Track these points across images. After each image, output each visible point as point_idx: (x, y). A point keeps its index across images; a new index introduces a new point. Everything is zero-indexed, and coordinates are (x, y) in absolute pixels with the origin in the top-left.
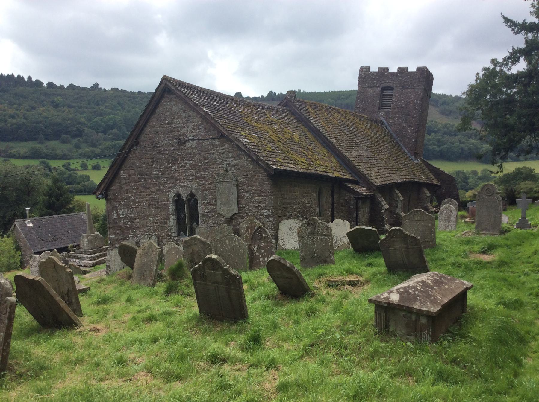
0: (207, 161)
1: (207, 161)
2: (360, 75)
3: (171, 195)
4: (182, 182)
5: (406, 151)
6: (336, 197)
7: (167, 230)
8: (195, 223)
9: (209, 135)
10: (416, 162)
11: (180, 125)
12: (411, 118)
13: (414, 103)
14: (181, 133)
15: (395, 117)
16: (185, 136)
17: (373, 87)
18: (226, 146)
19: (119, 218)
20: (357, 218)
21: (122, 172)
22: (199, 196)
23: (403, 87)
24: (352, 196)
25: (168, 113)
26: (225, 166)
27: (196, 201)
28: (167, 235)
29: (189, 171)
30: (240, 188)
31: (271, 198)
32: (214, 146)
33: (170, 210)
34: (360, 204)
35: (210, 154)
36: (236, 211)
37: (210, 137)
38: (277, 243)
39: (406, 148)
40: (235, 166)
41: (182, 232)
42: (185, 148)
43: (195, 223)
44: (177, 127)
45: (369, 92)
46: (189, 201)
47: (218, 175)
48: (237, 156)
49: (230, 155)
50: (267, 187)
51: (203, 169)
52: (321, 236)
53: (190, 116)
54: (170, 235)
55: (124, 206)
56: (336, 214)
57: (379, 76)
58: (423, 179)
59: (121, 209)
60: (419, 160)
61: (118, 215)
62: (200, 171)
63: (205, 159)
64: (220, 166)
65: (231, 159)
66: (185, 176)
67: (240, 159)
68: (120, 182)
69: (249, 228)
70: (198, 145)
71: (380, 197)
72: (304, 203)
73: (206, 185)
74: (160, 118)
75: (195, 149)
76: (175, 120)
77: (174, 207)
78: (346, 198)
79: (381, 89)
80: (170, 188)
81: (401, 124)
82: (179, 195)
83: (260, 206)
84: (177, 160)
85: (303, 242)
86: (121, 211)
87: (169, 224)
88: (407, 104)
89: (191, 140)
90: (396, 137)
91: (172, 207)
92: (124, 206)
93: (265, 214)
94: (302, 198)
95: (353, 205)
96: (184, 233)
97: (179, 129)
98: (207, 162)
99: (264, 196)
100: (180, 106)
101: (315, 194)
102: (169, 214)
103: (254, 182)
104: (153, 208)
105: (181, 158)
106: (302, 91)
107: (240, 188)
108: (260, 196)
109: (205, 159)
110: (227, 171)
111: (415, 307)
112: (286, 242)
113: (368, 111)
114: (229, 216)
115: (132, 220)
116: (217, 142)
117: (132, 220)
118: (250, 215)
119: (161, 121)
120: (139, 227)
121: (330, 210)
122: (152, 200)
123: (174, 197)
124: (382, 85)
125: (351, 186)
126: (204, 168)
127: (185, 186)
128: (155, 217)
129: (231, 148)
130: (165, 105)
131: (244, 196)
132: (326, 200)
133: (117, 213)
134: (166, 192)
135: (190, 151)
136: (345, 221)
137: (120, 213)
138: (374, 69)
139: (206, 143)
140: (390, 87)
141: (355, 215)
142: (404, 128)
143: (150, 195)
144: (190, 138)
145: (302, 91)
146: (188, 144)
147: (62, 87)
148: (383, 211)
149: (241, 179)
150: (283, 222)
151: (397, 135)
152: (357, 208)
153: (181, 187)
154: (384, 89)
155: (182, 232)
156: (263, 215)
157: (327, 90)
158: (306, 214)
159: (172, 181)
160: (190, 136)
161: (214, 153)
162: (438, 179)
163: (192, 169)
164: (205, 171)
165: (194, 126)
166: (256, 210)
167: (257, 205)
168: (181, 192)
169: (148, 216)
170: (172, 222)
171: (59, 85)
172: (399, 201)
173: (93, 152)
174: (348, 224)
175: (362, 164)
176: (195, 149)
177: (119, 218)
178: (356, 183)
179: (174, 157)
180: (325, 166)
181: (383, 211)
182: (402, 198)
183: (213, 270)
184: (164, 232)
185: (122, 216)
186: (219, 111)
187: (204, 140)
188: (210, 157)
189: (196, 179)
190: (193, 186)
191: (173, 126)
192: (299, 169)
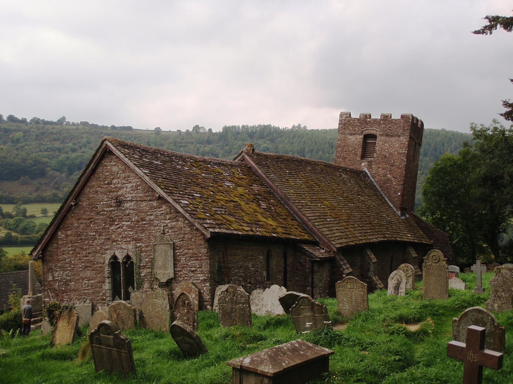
0: (144, 222)
1: (144, 222)
2: (340, 121)
3: (108, 257)
4: (119, 244)
5: (392, 206)
6: (290, 260)
7: (101, 294)
8: (130, 287)
9: (147, 196)
10: (403, 218)
11: (119, 185)
12: (396, 169)
13: (398, 153)
14: (120, 193)
15: (379, 167)
16: (124, 196)
17: (354, 134)
18: (164, 207)
19: (54, 280)
20: (313, 282)
21: (59, 233)
23: (387, 135)
24: (308, 259)
25: (108, 174)
26: (162, 228)
28: (101, 299)
29: (126, 233)
30: (177, 251)
31: (207, 262)
32: (152, 207)
33: (106, 273)
34: (316, 268)
35: (148, 215)
36: (172, 276)
37: (149, 198)
38: (212, 309)
39: (391, 202)
40: (172, 228)
41: (117, 296)
42: (123, 208)
43: (130, 287)
44: (117, 187)
46: (125, 263)
47: (155, 237)
48: (175, 218)
49: (168, 217)
50: (204, 251)
51: (141, 230)
52: (240, 303)
53: (129, 177)
54: (105, 300)
55: (60, 267)
57: (360, 123)
58: (408, 237)
59: (57, 271)
60: (407, 216)
61: (54, 277)
62: (136, 233)
63: (143, 220)
64: (157, 228)
65: (169, 221)
66: (122, 238)
67: (177, 221)
68: (57, 243)
70: (136, 206)
71: (342, 260)
72: (248, 267)
73: (143, 248)
74: (100, 178)
75: (134, 210)
76: (115, 181)
77: (109, 269)
78: (302, 261)
79: (363, 136)
80: (107, 249)
81: (385, 176)
82: (115, 257)
83: (196, 270)
84: (114, 221)
85: (222, 309)
86: (57, 274)
87: (104, 287)
88: (391, 154)
89: (129, 201)
90: (380, 190)
91: (107, 269)
92: (60, 267)
93: (201, 278)
94: (245, 262)
95: (308, 269)
96: (119, 297)
98: (145, 224)
99: (201, 260)
100: (120, 167)
101: (261, 257)
103: (191, 245)
104: (88, 270)
105: (119, 219)
107: (177, 251)
109: (143, 220)
110: (164, 234)
111: (259, 369)
114: (164, 280)
115: (66, 283)
116: (155, 204)
117: (66, 283)
118: (186, 280)
119: (100, 181)
120: (74, 290)
121: (282, 274)
122: (88, 262)
123: (110, 259)
124: (365, 133)
126: (142, 230)
127: (121, 248)
128: (90, 280)
129: (168, 210)
130: (106, 166)
131: (180, 260)
132: (276, 262)
133: (53, 275)
134: (102, 254)
135: (127, 212)
136: (282, 287)
137: (56, 275)
138: (355, 115)
139: (144, 204)
141: (310, 280)
142: (388, 180)
143: (86, 256)
144: (128, 199)
146: (127, 205)
147: (24, 121)
148: (344, 275)
149: (178, 242)
151: (381, 188)
152: (313, 272)
153: (118, 249)
154: (367, 137)
155: (117, 296)
156: (199, 280)
159: (109, 242)
160: (129, 197)
161: (151, 215)
162: (430, 238)
163: (129, 231)
164: (142, 233)
165: (132, 186)
166: (193, 275)
167: (193, 269)
168: (118, 254)
169: (83, 279)
170: (107, 286)
171: (21, 119)
172: (371, 263)
173: (55, 195)
175: (326, 222)
176: (134, 210)
177: (54, 280)
179: (112, 218)
180: (271, 226)
181: (344, 275)
182: (375, 260)
183: (107, 335)
184: (98, 296)
185: (57, 278)
186: (161, 170)
187: (142, 201)
188: (147, 218)
189: (132, 241)
190: (130, 248)
191: (112, 186)
192: (245, 230)
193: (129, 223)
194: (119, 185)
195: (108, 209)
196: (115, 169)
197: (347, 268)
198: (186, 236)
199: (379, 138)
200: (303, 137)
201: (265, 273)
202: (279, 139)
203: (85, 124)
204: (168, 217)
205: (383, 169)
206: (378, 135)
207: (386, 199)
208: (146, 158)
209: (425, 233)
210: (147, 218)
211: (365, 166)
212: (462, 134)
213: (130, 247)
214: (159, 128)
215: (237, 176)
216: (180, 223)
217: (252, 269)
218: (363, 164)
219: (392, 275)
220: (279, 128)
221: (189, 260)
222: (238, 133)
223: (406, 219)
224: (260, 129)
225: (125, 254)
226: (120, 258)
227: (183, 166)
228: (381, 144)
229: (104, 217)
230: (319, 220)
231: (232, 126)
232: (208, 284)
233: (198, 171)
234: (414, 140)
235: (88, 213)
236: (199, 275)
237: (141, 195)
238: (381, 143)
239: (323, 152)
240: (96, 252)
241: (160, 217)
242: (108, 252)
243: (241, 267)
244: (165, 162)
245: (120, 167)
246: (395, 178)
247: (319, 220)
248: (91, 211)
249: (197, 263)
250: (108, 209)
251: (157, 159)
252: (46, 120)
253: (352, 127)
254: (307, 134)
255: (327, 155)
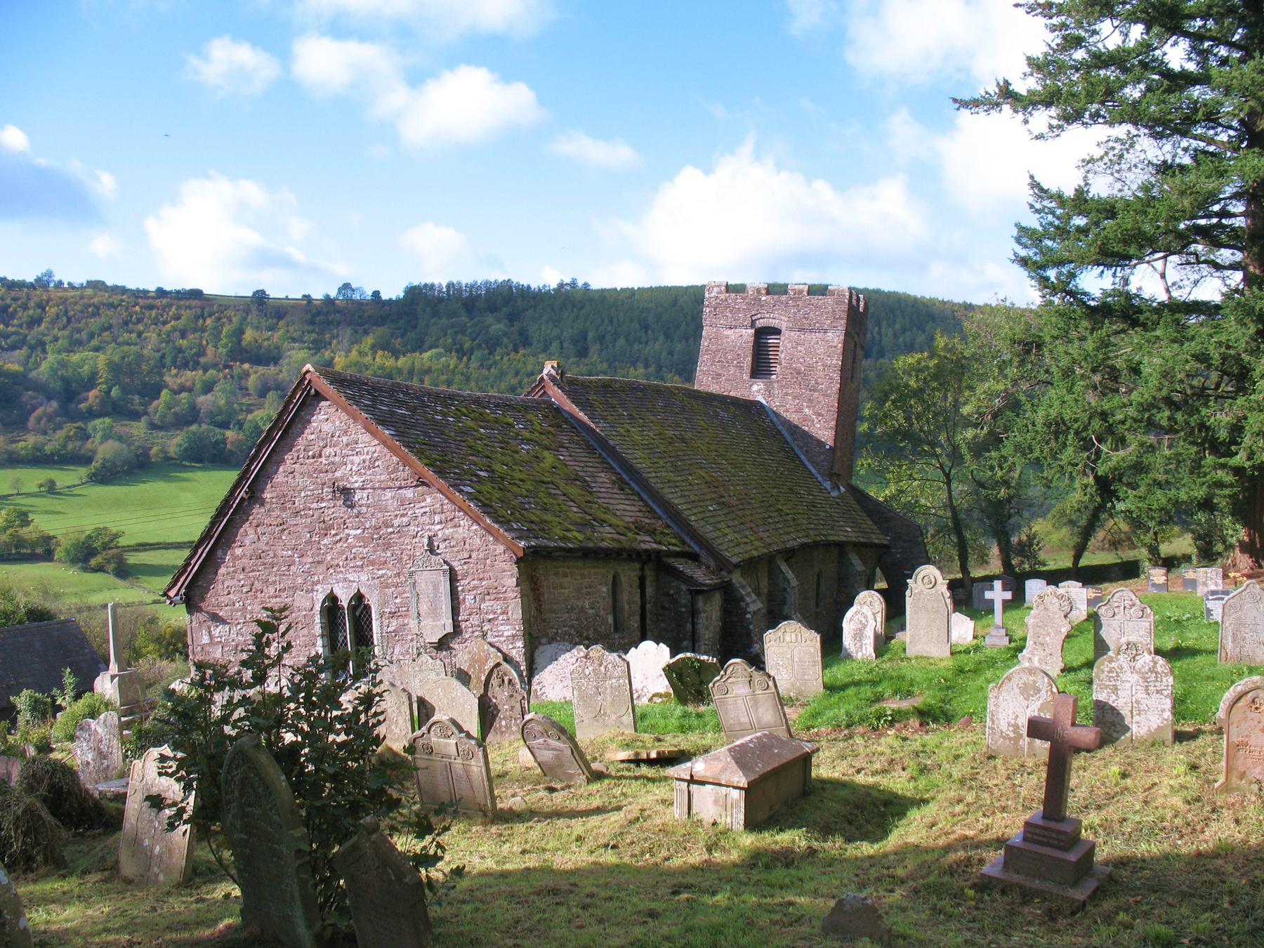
0: (390, 530)
1: (390, 530)
5: (813, 471)
6: (650, 590)
12: (821, 398)
14: (338, 474)
15: (787, 394)
18: (428, 500)
20: (694, 632)
22: (373, 600)
24: (684, 587)
26: (426, 541)
27: (367, 608)
34: (700, 604)
36: (450, 629)
37: (398, 484)
39: (812, 463)
45: (727, 337)
46: (353, 609)
49: (437, 518)
56: (649, 634)
58: (847, 533)
60: (843, 489)
69: (476, 661)
72: (582, 607)
76: (328, 451)
80: (318, 582)
81: (799, 410)
82: (332, 598)
88: (810, 367)
90: (789, 439)
93: (506, 634)
97: (334, 467)
100: (337, 423)
101: (604, 589)
102: (314, 636)
106: (580, 283)
108: (497, 599)
112: (547, 690)
113: (727, 380)
116: (409, 493)
121: (637, 618)
123: (324, 601)
124: (759, 324)
125: (671, 560)
127: (345, 580)
133: (210, 632)
139: (389, 494)
140: (774, 328)
141: (689, 627)
144: (357, 485)
145: (580, 283)
148: (748, 616)
150: (541, 648)
157: (646, 284)
158: (588, 630)
159: (321, 568)
162: (885, 532)
167: (491, 616)
174: (664, 649)
178: (694, 557)
181: (748, 616)
188: (396, 522)
193: (359, 531)
194: (337, 459)
195: (314, 505)
196: (327, 427)
197: (754, 602)
198: (474, 555)
199: (786, 334)
200: (583, 308)
201: (610, 619)
202: (530, 312)
203: (97, 285)
204: (437, 518)
205: (795, 398)
206: (783, 329)
207: (803, 458)
208: (382, 403)
209: (875, 523)
210: (396, 522)
211: (758, 391)
212: (915, 299)
213: (364, 577)
214: (263, 292)
215: (538, 428)
216: (460, 530)
217: (591, 611)
218: (755, 388)
219: (849, 614)
220: (529, 287)
221: (483, 600)
222: (441, 300)
223: (841, 497)
224: (488, 290)
225: (353, 592)
226: (344, 599)
227: (445, 415)
228: (785, 348)
229: (309, 520)
230: (695, 511)
231: (426, 285)
232: (520, 644)
233: (471, 424)
234: (853, 338)
235: (277, 512)
236: (501, 628)
237: (383, 478)
238: (789, 345)
239: (627, 340)
240: (294, 589)
241: (422, 520)
242: (318, 587)
243: (573, 609)
244: (413, 410)
245: (337, 423)
246: (819, 415)
247: (695, 511)
248: (284, 510)
249: (498, 606)
250: (314, 505)
251: (401, 404)
252: (10, 278)
253: (731, 311)
254: (591, 300)
255: (636, 347)
